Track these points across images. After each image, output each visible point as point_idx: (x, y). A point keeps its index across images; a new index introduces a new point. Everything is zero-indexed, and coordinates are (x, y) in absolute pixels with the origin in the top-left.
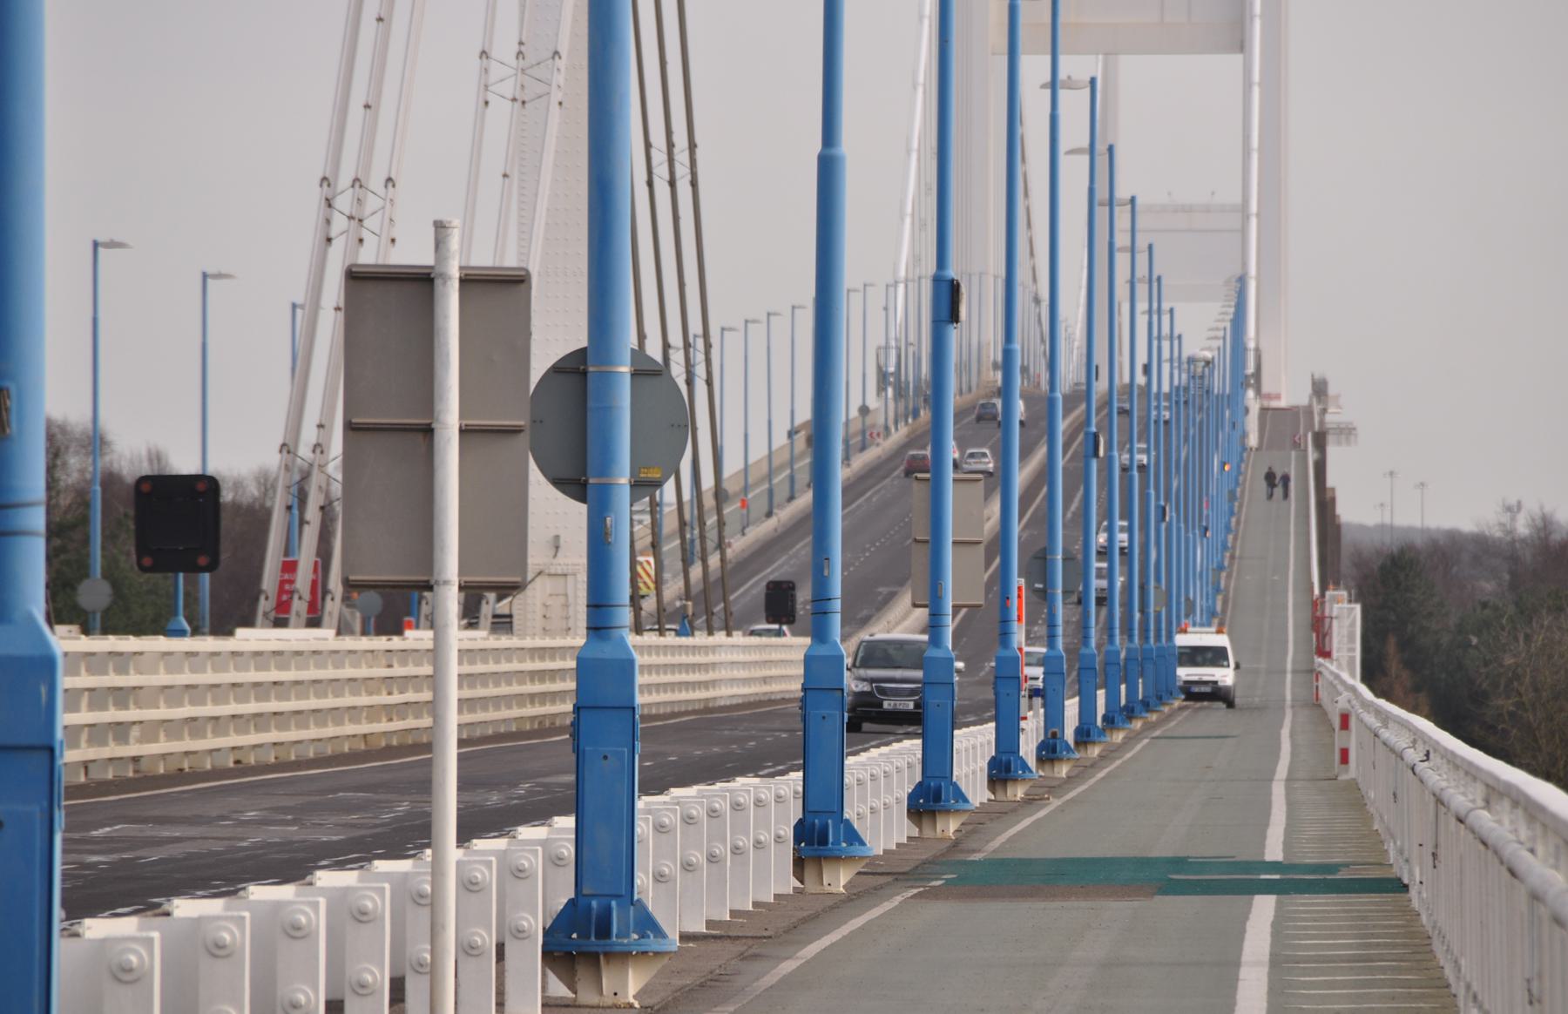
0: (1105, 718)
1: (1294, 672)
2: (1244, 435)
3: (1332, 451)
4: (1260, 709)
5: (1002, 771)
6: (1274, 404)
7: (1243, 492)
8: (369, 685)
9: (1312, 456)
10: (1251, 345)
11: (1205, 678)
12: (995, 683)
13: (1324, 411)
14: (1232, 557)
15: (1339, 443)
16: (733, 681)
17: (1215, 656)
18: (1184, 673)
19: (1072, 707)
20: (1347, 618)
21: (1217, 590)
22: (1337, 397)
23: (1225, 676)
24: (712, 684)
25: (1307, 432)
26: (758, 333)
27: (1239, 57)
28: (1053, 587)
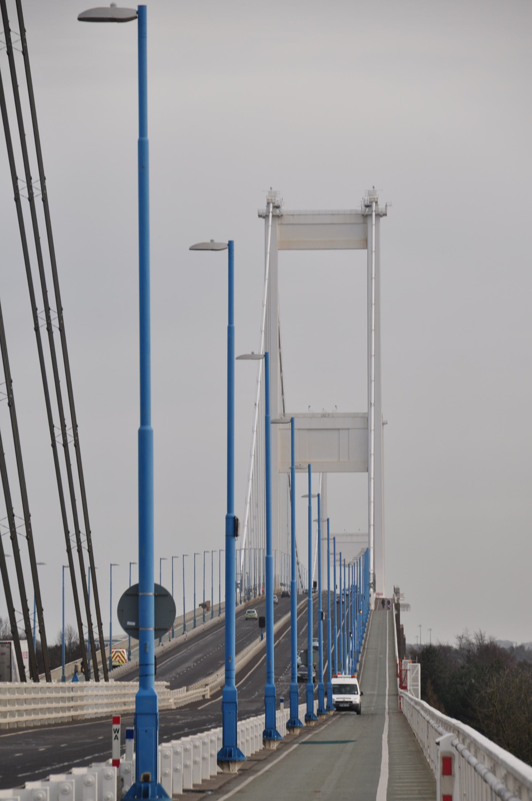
0: (327, 706)
1: (389, 695)
2: (369, 604)
3: (402, 613)
4: (373, 715)
5: (292, 724)
6: (381, 597)
7: (368, 625)
8: (57, 700)
9: (395, 613)
10: (372, 572)
11: (346, 700)
12: (223, 706)
13: (398, 599)
14: (364, 648)
15: (404, 610)
16: (96, 705)
17: (349, 689)
18: (336, 697)
19: (316, 703)
20: (414, 671)
21: (358, 661)
22: (403, 594)
23: (356, 699)
24: (82, 707)
25: (392, 606)
26: (178, 562)
27: (367, 474)
28: (145, 624)
